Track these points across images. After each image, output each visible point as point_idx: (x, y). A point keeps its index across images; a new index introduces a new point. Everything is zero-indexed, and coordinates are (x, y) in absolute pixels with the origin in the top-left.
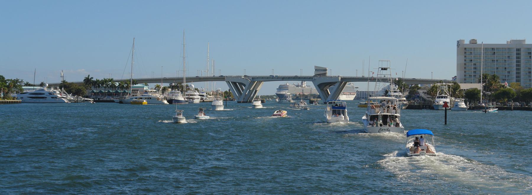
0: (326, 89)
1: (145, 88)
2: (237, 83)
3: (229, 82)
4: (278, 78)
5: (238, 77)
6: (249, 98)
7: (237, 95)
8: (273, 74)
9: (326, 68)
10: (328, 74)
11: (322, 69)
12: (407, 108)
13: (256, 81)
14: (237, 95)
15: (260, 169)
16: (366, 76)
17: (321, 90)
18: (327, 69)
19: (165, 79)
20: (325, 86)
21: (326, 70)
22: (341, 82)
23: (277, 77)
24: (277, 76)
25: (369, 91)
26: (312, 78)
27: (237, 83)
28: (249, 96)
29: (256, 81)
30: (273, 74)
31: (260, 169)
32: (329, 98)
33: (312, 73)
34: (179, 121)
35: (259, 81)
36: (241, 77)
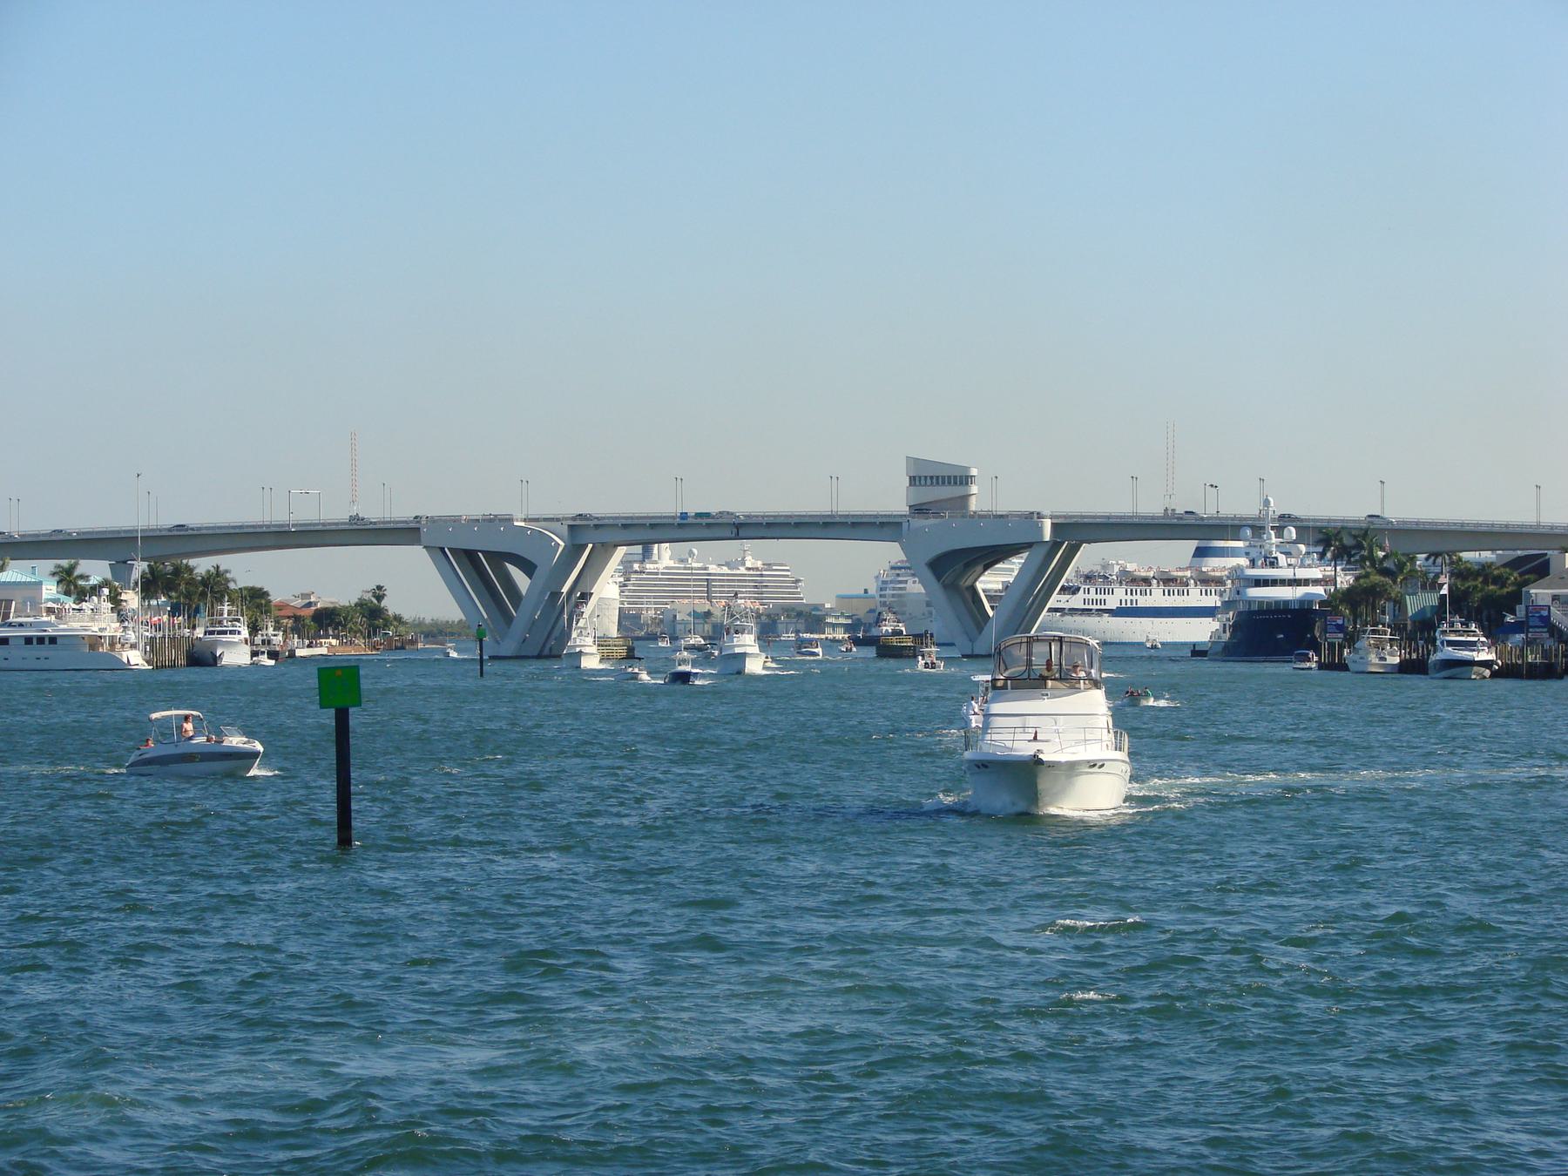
0: (968, 583)
1: (44, 591)
2: (480, 554)
3: (442, 549)
4: (709, 525)
5: (491, 521)
6: (548, 637)
7: (486, 616)
8: (679, 505)
9: (967, 469)
10: (979, 499)
11: (946, 474)
12: (1494, 675)
13: (590, 546)
14: (486, 616)
15: (1111, 1166)
16: (374, 512)
17: (945, 587)
18: (974, 472)
19: (61, 537)
20: (969, 565)
21: (964, 479)
22: (1055, 546)
23: (705, 521)
24: (707, 515)
25: (1297, 577)
26: (900, 524)
27: (480, 554)
28: (550, 627)
29: (590, 546)
30: (679, 505)
31: (1111, 1166)
32: (992, 630)
33: (894, 499)
34: (1034, 810)
35: (603, 544)
36: (509, 520)
